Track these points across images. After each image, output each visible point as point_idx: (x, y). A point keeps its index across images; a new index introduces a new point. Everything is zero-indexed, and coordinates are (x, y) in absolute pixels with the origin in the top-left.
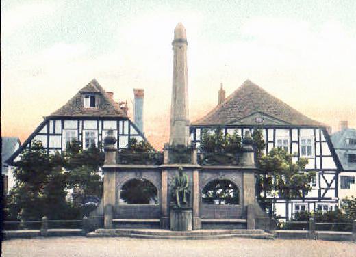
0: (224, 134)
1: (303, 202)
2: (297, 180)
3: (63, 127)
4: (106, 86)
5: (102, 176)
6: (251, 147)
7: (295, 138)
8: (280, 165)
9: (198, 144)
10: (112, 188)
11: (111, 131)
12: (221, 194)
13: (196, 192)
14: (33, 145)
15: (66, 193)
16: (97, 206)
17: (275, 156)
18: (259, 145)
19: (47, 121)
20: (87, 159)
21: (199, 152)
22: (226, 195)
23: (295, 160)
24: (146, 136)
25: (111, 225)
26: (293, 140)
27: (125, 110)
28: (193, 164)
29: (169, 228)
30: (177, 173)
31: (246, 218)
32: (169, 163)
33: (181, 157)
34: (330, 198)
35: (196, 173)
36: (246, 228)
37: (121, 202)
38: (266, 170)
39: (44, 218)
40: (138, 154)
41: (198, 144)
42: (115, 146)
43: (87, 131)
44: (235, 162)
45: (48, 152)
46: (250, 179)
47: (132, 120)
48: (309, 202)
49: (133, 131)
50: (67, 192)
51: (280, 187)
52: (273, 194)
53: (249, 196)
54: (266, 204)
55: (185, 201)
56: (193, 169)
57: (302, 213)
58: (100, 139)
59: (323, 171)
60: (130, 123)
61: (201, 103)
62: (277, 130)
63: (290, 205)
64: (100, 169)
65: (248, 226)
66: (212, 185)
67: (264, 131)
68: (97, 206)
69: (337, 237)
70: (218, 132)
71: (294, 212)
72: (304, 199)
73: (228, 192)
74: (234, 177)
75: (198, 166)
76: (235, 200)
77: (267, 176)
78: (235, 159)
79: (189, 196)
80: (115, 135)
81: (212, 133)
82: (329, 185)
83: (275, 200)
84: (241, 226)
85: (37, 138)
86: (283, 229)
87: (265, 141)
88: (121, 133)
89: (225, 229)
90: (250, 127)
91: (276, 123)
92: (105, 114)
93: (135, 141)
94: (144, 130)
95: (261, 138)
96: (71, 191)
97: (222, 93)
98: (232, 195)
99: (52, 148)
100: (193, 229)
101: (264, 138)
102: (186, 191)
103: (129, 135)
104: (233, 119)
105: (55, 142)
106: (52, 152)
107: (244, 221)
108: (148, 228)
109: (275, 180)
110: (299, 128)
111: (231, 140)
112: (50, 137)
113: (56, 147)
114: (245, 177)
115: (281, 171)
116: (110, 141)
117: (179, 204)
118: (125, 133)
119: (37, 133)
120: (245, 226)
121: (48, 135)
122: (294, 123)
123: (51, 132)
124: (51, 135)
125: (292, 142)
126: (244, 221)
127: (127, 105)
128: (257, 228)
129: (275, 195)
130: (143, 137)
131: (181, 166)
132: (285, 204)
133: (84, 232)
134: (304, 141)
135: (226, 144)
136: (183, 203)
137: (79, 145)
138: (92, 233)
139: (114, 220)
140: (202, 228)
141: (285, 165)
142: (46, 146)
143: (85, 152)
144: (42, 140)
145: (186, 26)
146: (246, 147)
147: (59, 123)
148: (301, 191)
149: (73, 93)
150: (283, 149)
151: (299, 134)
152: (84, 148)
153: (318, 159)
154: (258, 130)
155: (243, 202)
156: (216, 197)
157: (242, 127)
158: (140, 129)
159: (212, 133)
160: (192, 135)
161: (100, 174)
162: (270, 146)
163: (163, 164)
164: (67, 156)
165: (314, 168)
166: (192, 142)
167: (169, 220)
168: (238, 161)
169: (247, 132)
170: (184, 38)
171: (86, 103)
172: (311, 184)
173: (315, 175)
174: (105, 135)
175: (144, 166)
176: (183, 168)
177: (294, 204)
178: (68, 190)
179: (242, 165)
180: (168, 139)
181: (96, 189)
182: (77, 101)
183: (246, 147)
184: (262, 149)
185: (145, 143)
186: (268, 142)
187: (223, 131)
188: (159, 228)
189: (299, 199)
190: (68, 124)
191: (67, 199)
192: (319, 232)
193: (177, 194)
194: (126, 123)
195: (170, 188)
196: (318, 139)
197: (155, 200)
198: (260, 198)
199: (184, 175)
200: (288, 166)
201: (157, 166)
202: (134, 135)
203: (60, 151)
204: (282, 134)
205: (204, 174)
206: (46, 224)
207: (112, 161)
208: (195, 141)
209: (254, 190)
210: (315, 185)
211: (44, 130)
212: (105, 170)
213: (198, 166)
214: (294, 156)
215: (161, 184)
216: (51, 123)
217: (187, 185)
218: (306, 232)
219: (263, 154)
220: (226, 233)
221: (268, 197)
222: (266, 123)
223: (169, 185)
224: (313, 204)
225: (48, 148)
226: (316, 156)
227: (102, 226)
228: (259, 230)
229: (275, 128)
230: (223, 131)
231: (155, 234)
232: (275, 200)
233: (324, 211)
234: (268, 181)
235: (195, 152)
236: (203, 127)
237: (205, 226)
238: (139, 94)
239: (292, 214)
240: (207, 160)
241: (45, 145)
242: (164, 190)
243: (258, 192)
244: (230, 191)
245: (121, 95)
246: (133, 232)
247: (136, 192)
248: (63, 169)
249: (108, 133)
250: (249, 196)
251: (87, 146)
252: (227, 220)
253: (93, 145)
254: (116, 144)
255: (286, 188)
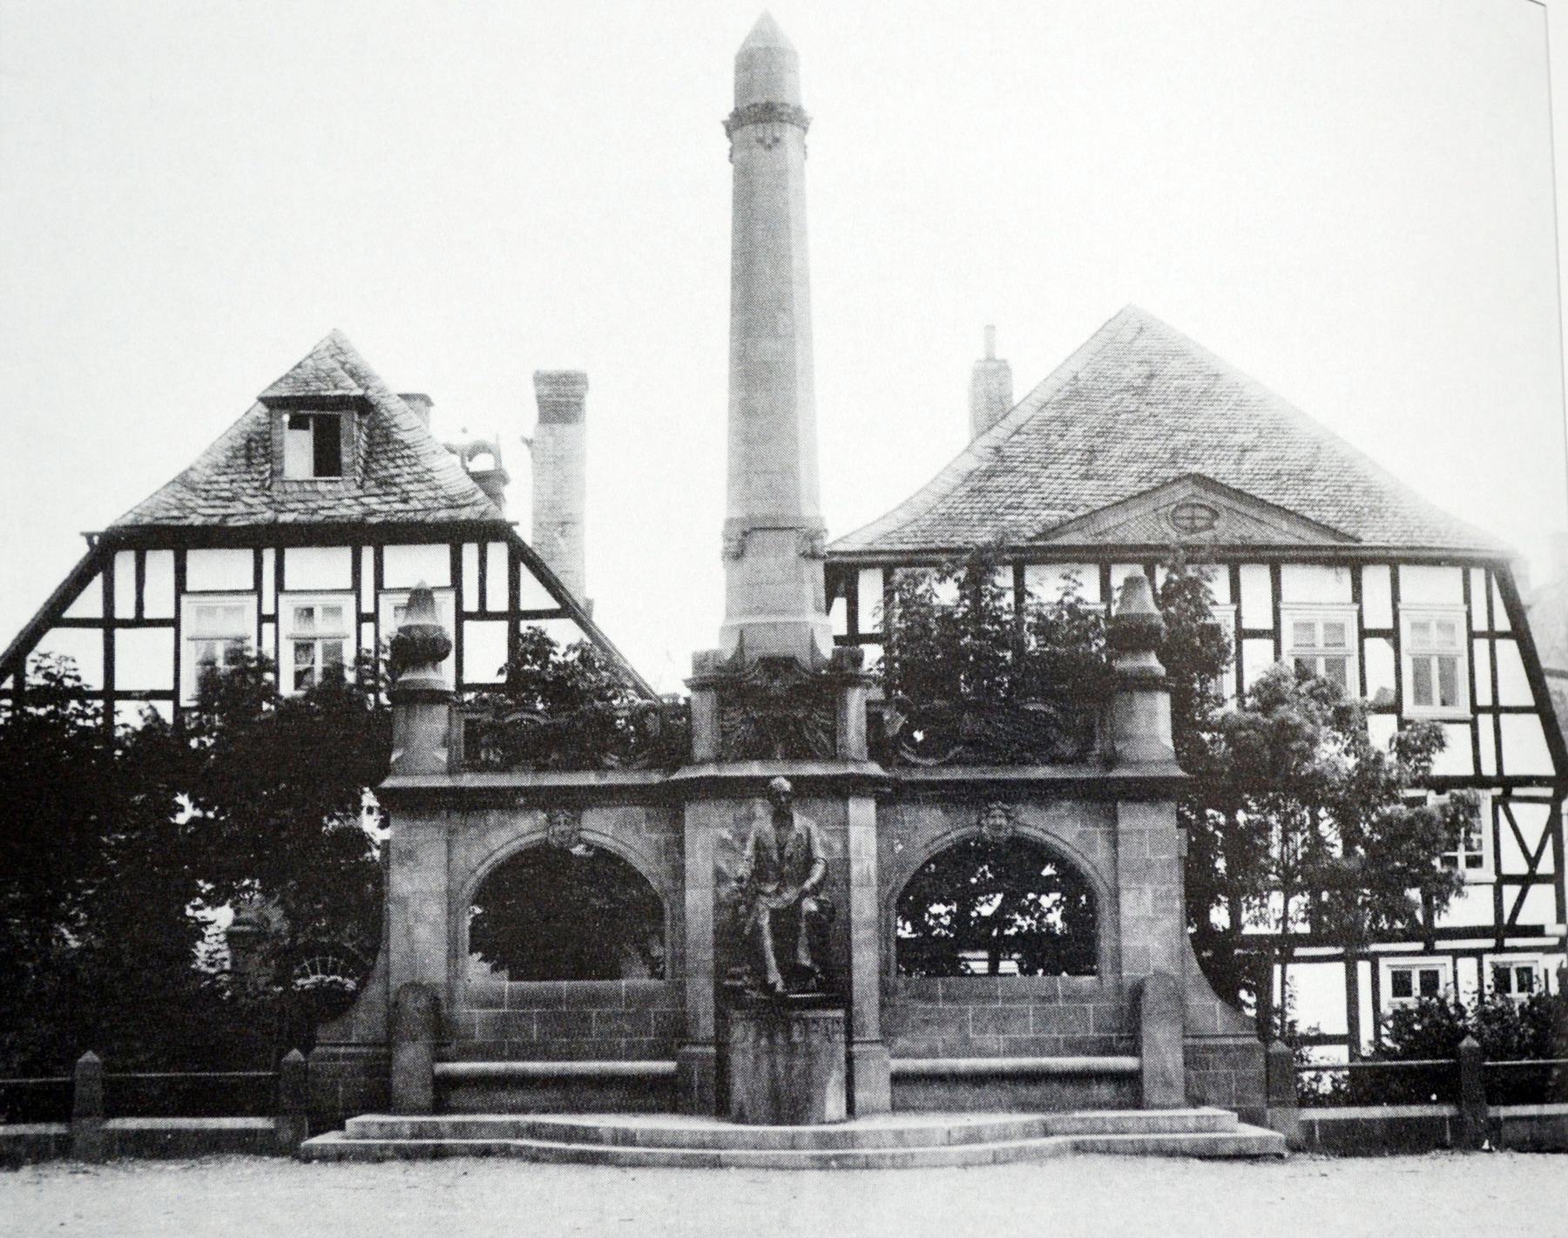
0: (1010, 598)
1: (1429, 951)
2: (1397, 833)
3: (181, 587)
4: (390, 374)
5: (380, 835)
6: (1152, 662)
7: (1378, 616)
8: (1307, 756)
9: (872, 654)
10: (426, 893)
11: (420, 598)
12: (1000, 919)
13: (864, 905)
14: (35, 680)
15: (198, 930)
16: (354, 996)
17: (1282, 711)
18: (1194, 653)
19: (100, 557)
20: (290, 758)
21: (877, 694)
22: (1024, 922)
23: (1382, 731)
24: (599, 619)
25: (425, 1097)
26: (1369, 624)
27: (488, 482)
28: (833, 757)
29: (721, 1108)
30: (761, 809)
31: (1135, 1051)
32: (719, 760)
33: (781, 724)
34: (1538, 931)
35: (863, 812)
36: (1138, 1107)
37: (477, 972)
38: (1255, 764)
39: (90, 1056)
40: (561, 711)
41: (872, 654)
42: (443, 676)
43: (305, 601)
44: (1068, 748)
45: (109, 713)
46: (1153, 834)
47: (525, 534)
48: (1457, 954)
49: (534, 595)
50: (207, 924)
51: (1307, 874)
52: (1273, 912)
53: (1147, 928)
54: (1233, 966)
55: (805, 960)
56: (841, 789)
57: (1424, 1010)
58: (368, 643)
59: (1507, 786)
60: (520, 555)
61: (880, 469)
62: (1289, 574)
63: (1364, 968)
64: (369, 799)
65: (1153, 1092)
66: (948, 872)
67: (1219, 586)
68: (354, 996)
69: (1524, 1131)
70: (974, 585)
71: (1386, 1010)
72: (1429, 937)
73: (1035, 903)
74: (1065, 830)
75: (874, 769)
76: (1073, 950)
77: (1241, 817)
78: (1064, 730)
79: (829, 931)
80: (443, 617)
81: (947, 594)
82: (1533, 862)
83: (1285, 947)
84: (1105, 1091)
85: (55, 642)
86: (1333, 1100)
87: (1229, 631)
88: (471, 604)
89: (1025, 1107)
90: (1149, 555)
91: (1281, 533)
92: (382, 508)
93: (542, 646)
94: (588, 586)
95: (1202, 611)
96: (223, 916)
97: (993, 372)
98: (1055, 918)
99: (127, 695)
100: (851, 1110)
101: (1222, 615)
102: (810, 905)
103: (514, 614)
104: (1052, 516)
105: (145, 662)
106: (130, 716)
107: (1128, 1063)
108: (619, 1109)
109: (1285, 840)
110: (1394, 560)
111: (1045, 629)
112: (119, 633)
113: (147, 687)
114: (1123, 825)
115: (1312, 790)
116: (417, 649)
117: (775, 977)
118: (492, 606)
119: (53, 615)
120: (1130, 1090)
121: (108, 623)
122: (1371, 537)
123: (125, 609)
124: (126, 624)
125: (1364, 634)
126: (1128, 1063)
127: (498, 459)
128: (1196, 1101)
129: (1285, 918)
130: (584, 624)
131: (780, 774)
132: (1340, 967)
133: (287, 1135)
134: (1422, 627)
135: (1019, 648)
136: (793, 973)
137: (258, 673)
138: (331, 1139)
139: (440, 1068)
140: (896, 1107)
141: (1332, 754)
142: (97, 684)
143: (289, 709)
144: (73, 653)
145: (796, 33)
146: (1126, 664)
147: (160, 563)
148: (1414, 894)
149: (232, 407)
150: (1321, 670)
151: (1396, 598)
152: (287, 689)
153: (1485, 721)
154: (1191, 572)
155: (1117, 967)
156: (970, 933)
157: (1104, 557)
158: (567, 581)
159: (947, 594)
160: (840, 604)
161: (369, 824)
162: (1258, 660)
163: (690, 761)
164: (198, 732)
165: (1469, 771)
166: (838, 640)
167: (722, 1064)
168: (1087, 735)
169: (1131, 583)
170: (787, 98)
171: (298, 452)
172: (1461, 854)
173: (1474, 809)
174: (391, 624)
175: (591, 779)
176: (796, 781)
177: (1383, 963)
178: (208, 913)
179: (1111, 760)
180: (709, 632)
181: (351, 898)
182: (256, 450)
183: (1126, 664)
184: (1214, 671)
185: (595, 655)
186: (1242, 634)
187: (1005, 578)
188: (674, 1110)
189: (1408, 937)
190: (208, 567)
191: (201, 964)
192: (1504, 1112)
193: (765, 921)
194: (498, 553)
195: (310, 362)
196: (1480, 624)
197: (645, 953)
198: (1205, 937)
199: (800, 821)
200: (1351, 762)
201: (656, 778)
202: (537, 615)
203: (166, 710)
204: (1315, 592)
205: (909, 814)
206: (98, 1091)
207: (427, 751)
208: (853, 638)
209: (1178, 889)
210: (1474, 862)
211: (89, 603)
212: (397, 805)
213: (874, 769)
214: (1380, 709)
215: (679, 873)
216: (124, 563)
217: (818, 872)
218: (1446, 1111)
219: (1220, 701)
220: (1028, 1133)
221: (1249, 930)
222: (1229, 530)
223: (720, 877)
224: (1473, 961)
225: (110, 694)
226: (1476, 709)
227: (382, 1101)
228: (1205, 1111)
229: (1275, 559)
230: (1005, 578)
231: (653, 1140)
232: (1285, 947)
233: (1518, 997)
234: (1245, 845)
235: (856, 702)
236: (899, 564)
237: (919, 1094)
238: (560, 401)
239: (1378, 1021)
240: (919, 736)
241: (94, 680)
242: (699, 901)
243: (1196, 910)
244: (1046, 901)
245: (461, 418)
246: (534, 1131)
247: (553, 918)
248: (182, 799)
249: (409, 607)
250: (1147, 928)
251: (300, 678)
252: (1028, 1062)
253: (334, 672)
254: (448, 664)
255: (1338, 880)
